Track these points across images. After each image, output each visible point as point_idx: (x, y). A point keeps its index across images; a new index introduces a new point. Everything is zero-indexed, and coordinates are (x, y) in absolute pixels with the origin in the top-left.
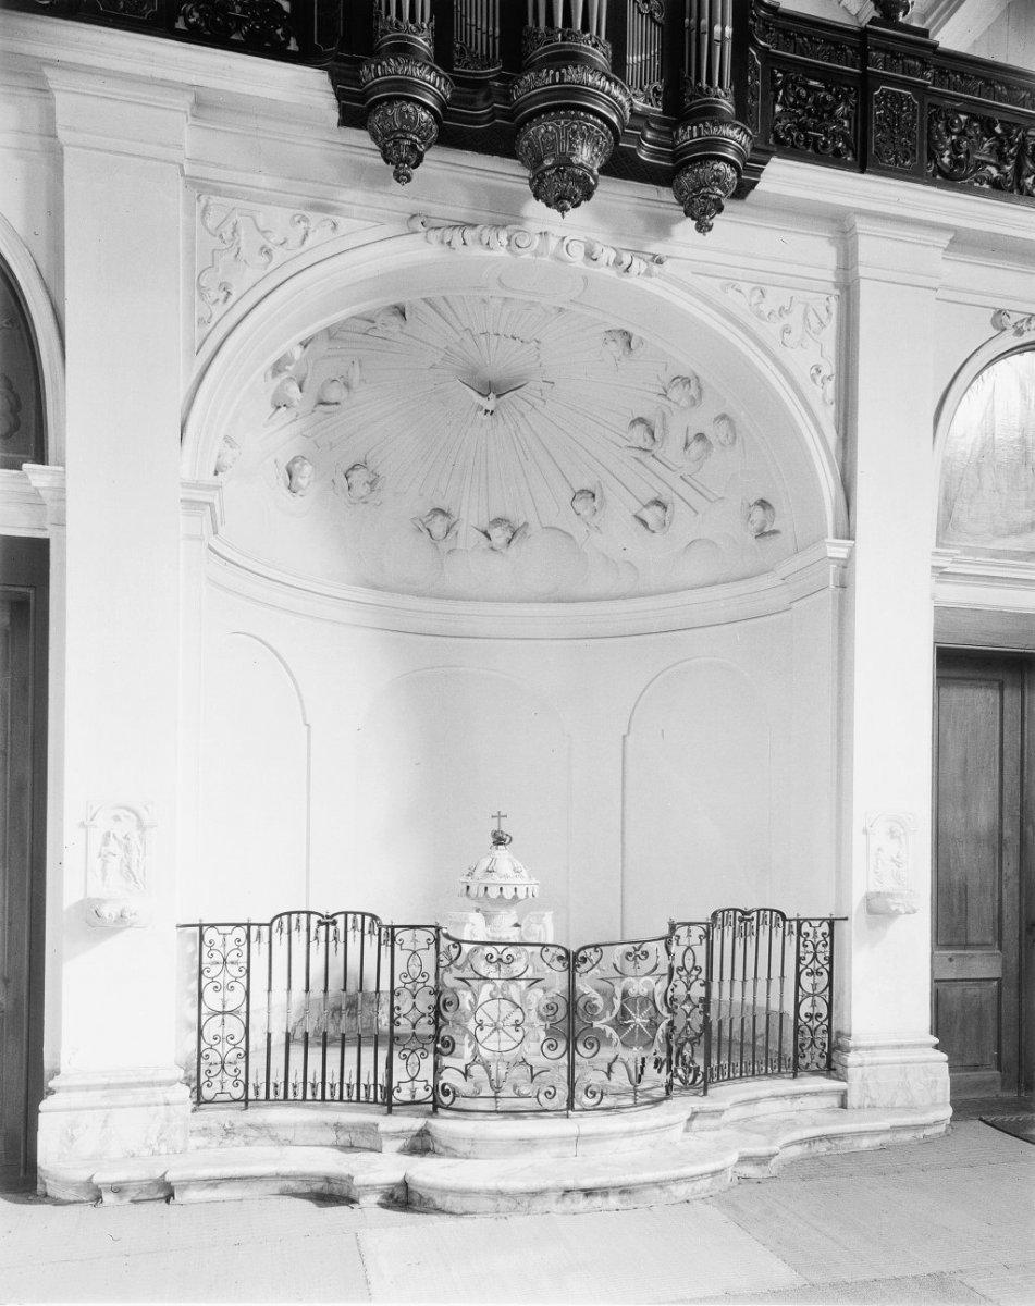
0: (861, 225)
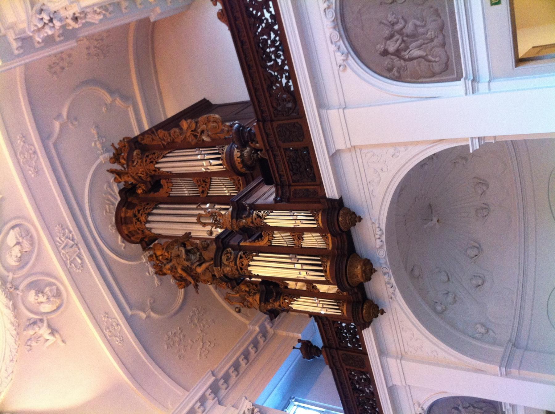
0: (331, 154)
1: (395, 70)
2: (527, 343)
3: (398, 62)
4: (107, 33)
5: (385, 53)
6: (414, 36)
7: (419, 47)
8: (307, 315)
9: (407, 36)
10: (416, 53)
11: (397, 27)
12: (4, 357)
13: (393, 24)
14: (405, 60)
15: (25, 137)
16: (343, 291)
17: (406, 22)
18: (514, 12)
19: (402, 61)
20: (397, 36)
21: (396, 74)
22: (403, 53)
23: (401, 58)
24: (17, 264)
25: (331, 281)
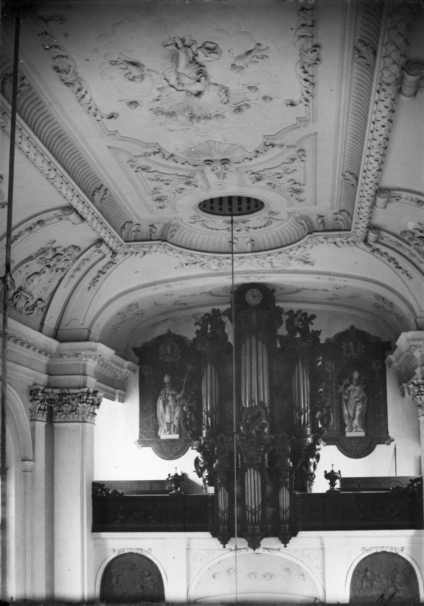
1: (358, 574)
2: (285, 236)
3: (361, 575)
4: (83, 365)
5: (366, 570)
6: (372, 585)
7: (367, 586)
8: (178, 237)
9: (372, 582)
10: (365, 584)
11: (377, 578)
12: (270, 169)
13: (378, 576)
14: (362, 579)
15: (110, 396)
16: (210, 485)
17: (379, 582)
18: (13, 159)
19: (361, 578)
20: (373, 577)
21: (357, 574)
22: (365, 579)
23: (363, 577)
24: (297, 333)
25: (123, 237)
